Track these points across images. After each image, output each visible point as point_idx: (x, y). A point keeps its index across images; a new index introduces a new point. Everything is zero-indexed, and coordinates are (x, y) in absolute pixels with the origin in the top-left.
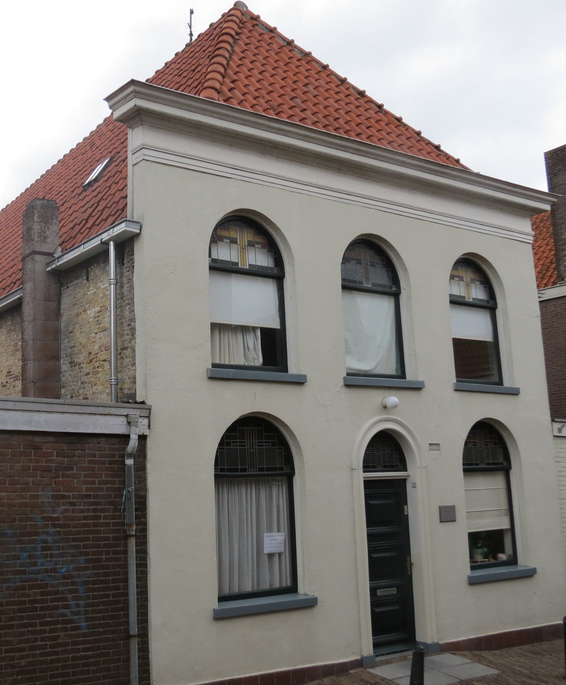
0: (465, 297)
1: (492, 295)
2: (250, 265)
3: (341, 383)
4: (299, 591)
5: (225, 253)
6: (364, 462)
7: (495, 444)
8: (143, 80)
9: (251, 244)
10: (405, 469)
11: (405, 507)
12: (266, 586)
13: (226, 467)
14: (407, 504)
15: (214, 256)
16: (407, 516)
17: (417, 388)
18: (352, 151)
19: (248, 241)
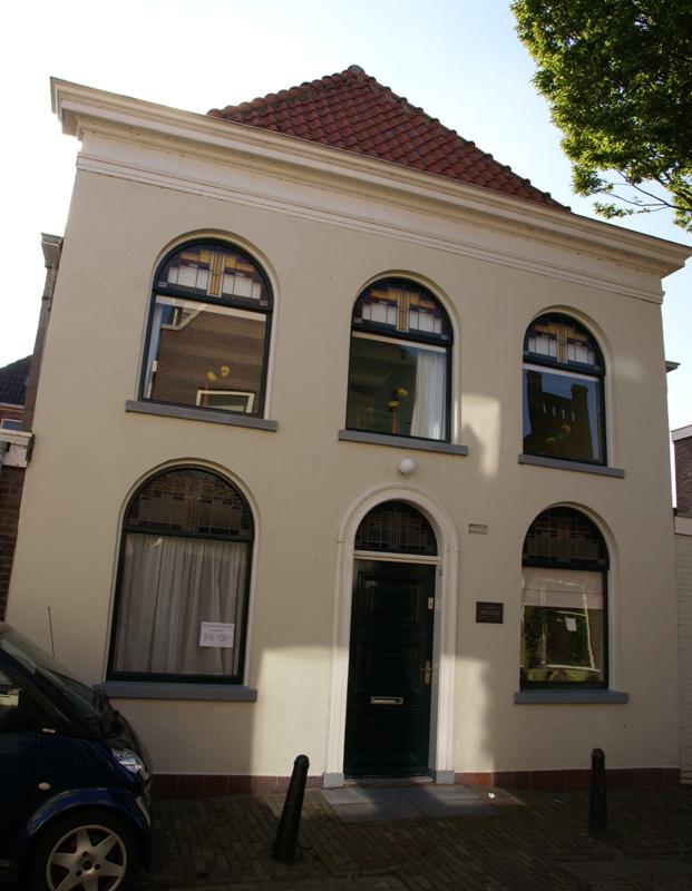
0: (395, 326)
1: (267, 291)
2: (223, 294)
3: (337, 437)
4: (610, 688)
5: (542, 347)
6: (357, 537)
7: (587, 537)
8: (204, 113)
9: (571, 341)
10: (435, 554)
11: (431, 600)
12: (189, 671)
13: (407, 544)
14: (433, 596)
15: (531, 349)
16: (432, 611)
17: (271, 428)
18: (316, 157)
19: (411, 305)
